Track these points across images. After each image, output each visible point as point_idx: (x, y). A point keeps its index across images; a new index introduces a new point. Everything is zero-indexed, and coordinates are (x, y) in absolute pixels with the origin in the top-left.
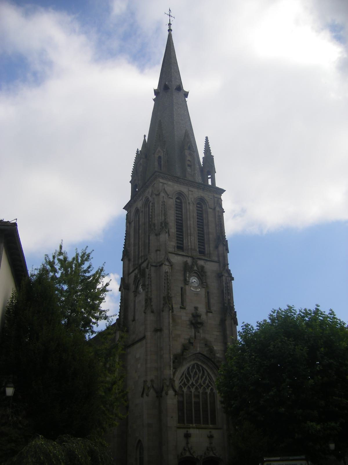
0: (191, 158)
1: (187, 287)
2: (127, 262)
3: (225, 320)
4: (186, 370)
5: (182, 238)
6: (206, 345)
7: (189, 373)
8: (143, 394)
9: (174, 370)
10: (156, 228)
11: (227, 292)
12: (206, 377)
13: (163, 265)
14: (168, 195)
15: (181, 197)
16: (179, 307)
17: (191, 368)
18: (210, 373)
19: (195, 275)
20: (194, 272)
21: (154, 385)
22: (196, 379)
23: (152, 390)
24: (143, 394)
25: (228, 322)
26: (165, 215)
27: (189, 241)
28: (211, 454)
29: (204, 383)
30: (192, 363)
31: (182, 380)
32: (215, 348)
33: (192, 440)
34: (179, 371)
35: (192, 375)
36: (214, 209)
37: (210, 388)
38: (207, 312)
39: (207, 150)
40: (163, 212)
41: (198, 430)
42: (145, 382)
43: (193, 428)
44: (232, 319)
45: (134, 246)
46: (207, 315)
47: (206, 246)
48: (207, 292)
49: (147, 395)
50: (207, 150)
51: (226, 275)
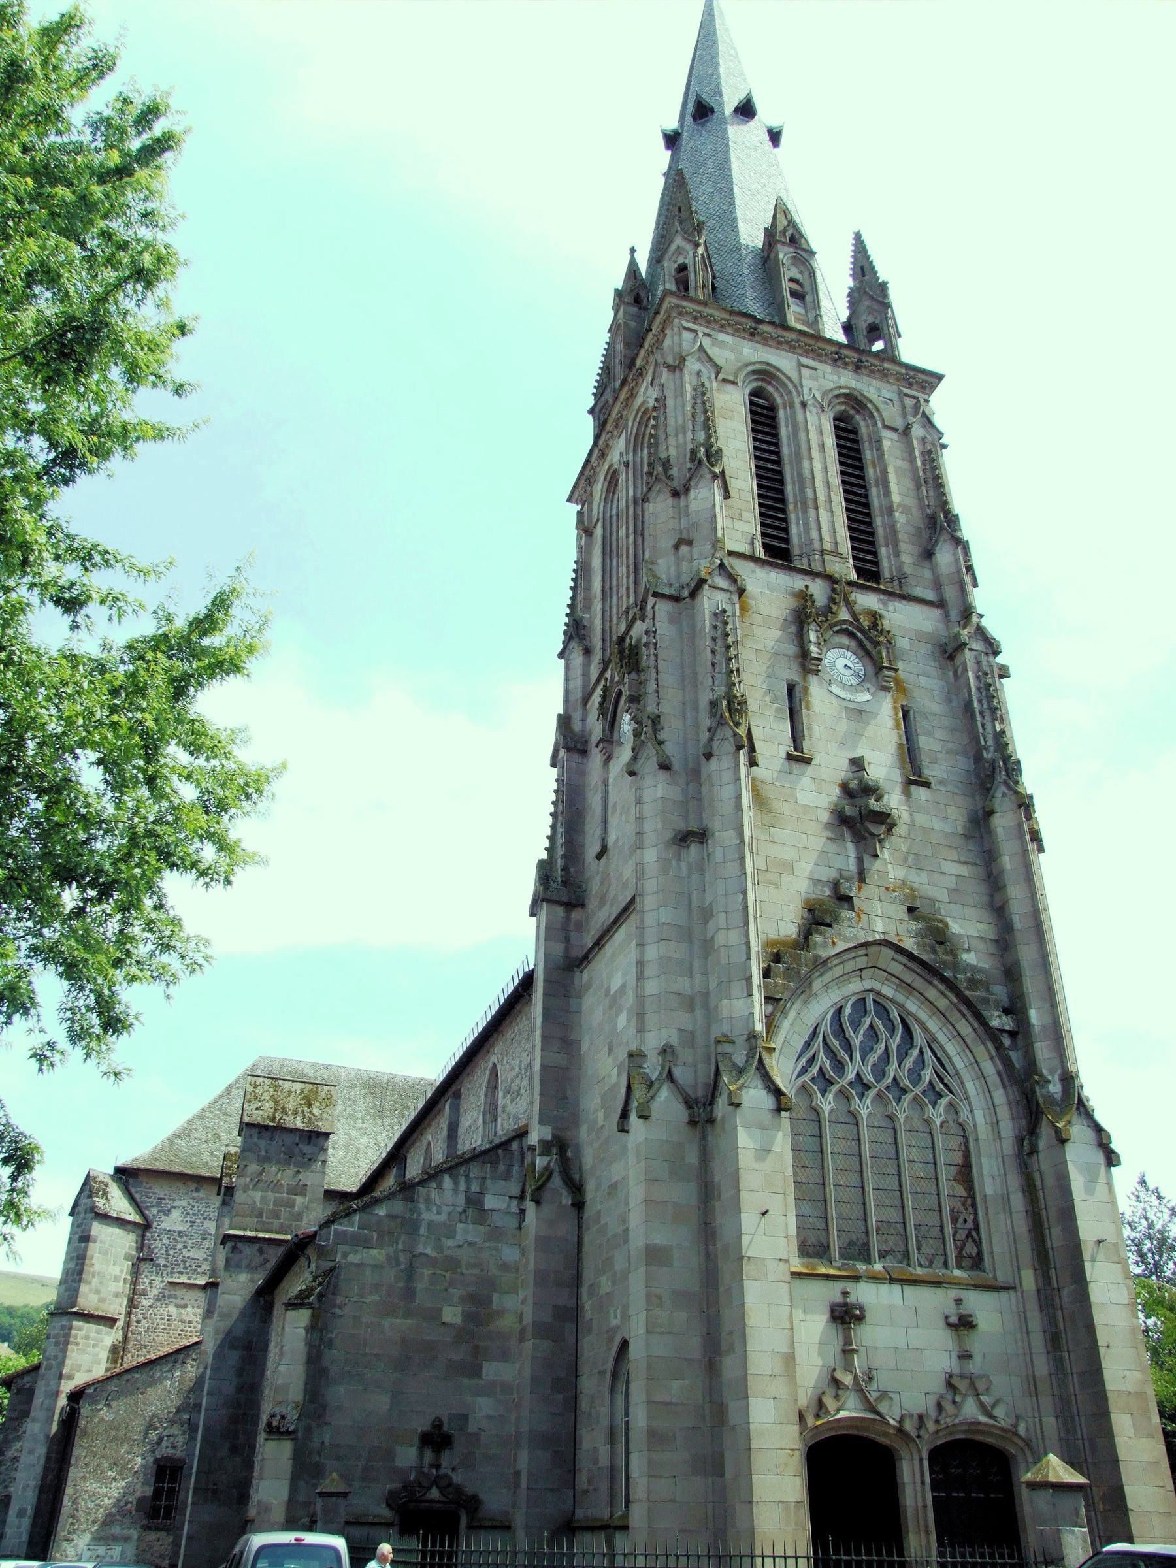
0: (801, 273)
1: (813, 681)
2: (577, 658)
3: (990, 813)
4: (829, 1016)
5: (785, 520)
6: (911, 910)
7: (840, 1031)
8: (625, 1115)
9: (770, 1008)
10: (674, 471)
11: (985, 706)
12: (921, 1052)
13: (706, 587)
14: (718, 370)
15: (770, 389)
16: (783, 755)
17: (848, 1010)
18: (941, 1037)
19: (845, 640)
20: (838, 632)
21: (677, 1072)
22: (873, 1058)
23: (665, 1094)
24: (625, 1115)
25: (1002, 822)
26: (708, 425)
27: (813, 525)
28: (970, 1410)
29: (916, 1078)
30: (855, 987)
31: (812, 1060)
32: (955, 927)
33: (867, 1335)
34: (792, 1014)
35: (857, 1040)
36: (906, 431)
37: (944, 1102)
38: (909, 783)
39: (863, 267)
40: (700, 418)
41: (896, 1288)
42: (635, 1057)
43: (874, 1278)
44: (1020, 806)
45: (604, 599)
46: (907, 793)
47: (883, 552)
48: (902, 707)
49: (644, 1117)
50: (863, 267)
51: (977, 645)
